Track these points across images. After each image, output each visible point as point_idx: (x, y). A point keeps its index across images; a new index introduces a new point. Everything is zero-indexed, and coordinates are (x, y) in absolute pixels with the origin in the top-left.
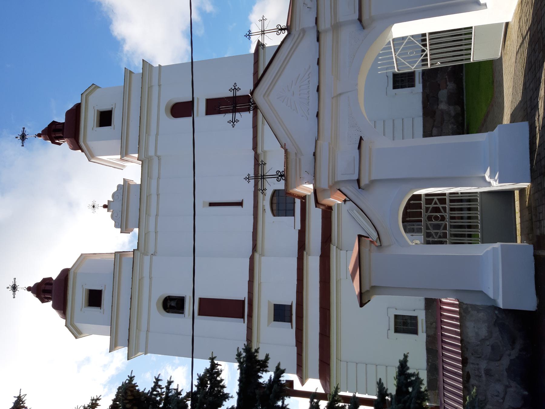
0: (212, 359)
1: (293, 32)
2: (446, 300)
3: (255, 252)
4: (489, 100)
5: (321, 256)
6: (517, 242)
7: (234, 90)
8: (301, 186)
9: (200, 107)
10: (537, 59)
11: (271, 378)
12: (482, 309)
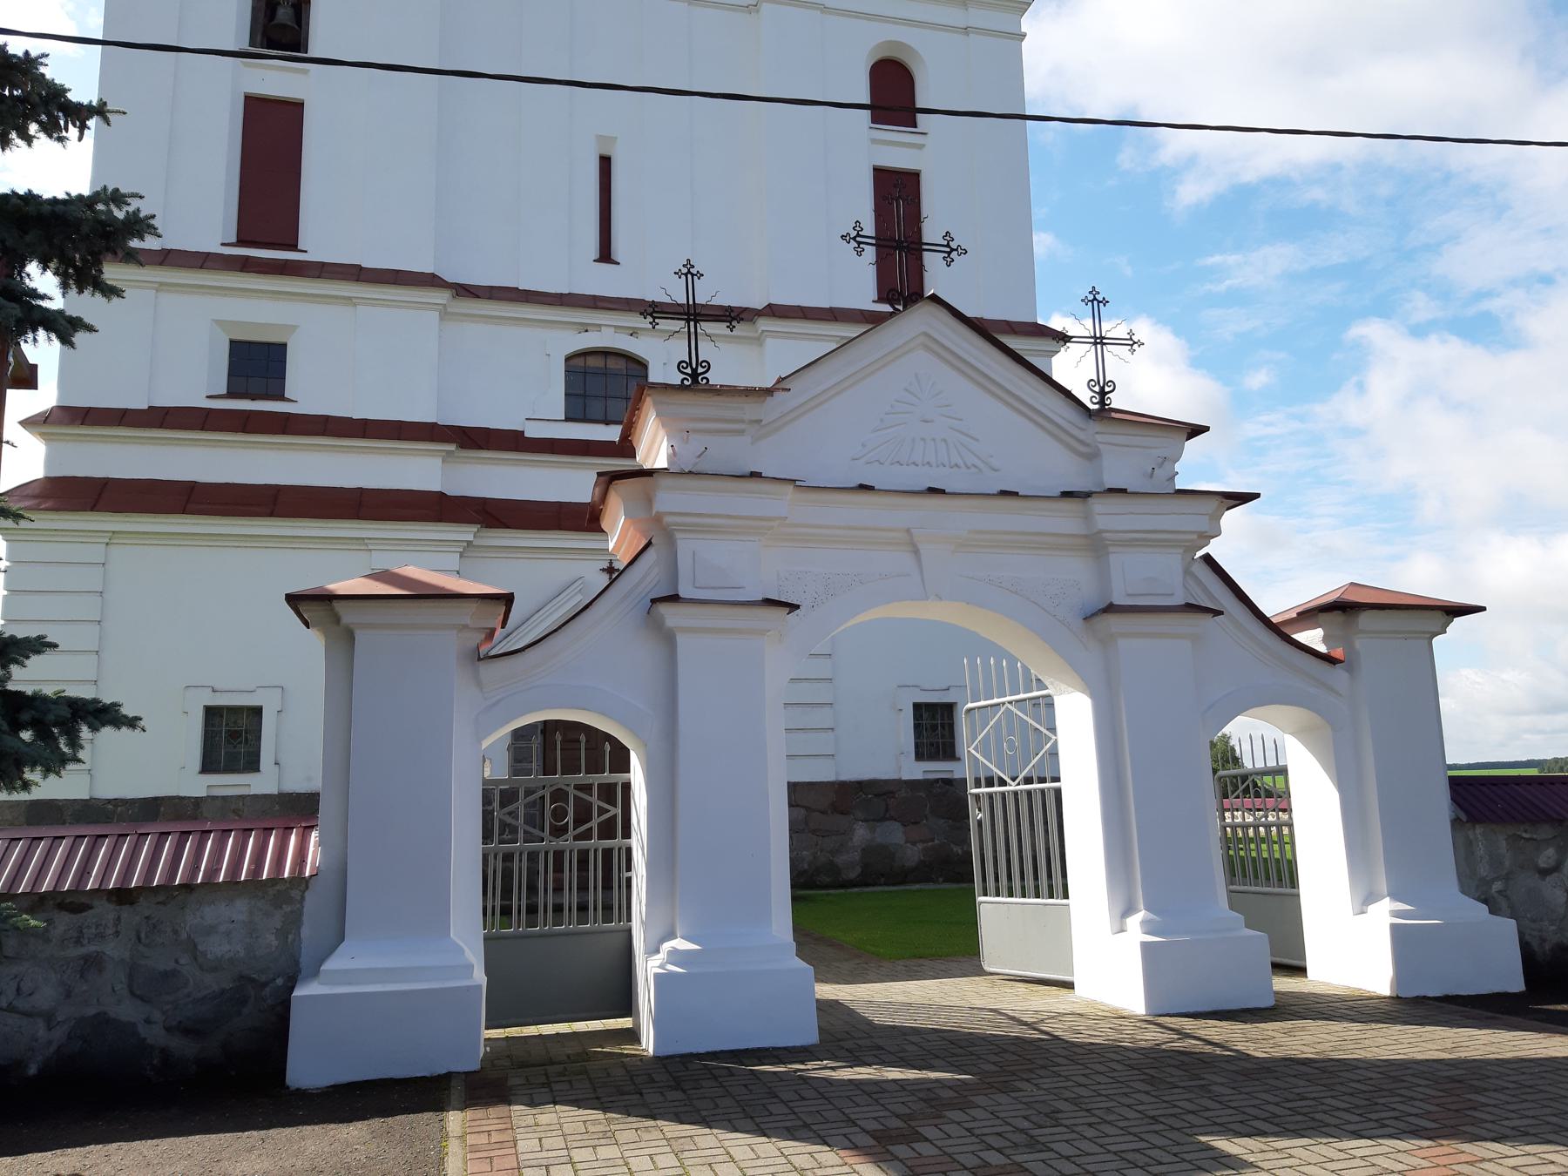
0: (100, 110)
1: (1094, 426)
2: (315, 842)
3: (454, 291)
4: (873, 949)
5: (441, 495)
6: (487, 1028)
7: (948, 246)
8: (662, 433)
9: (896, 149)
10: (980, 1058)
11: (44, 297)
12: (289, 940)
